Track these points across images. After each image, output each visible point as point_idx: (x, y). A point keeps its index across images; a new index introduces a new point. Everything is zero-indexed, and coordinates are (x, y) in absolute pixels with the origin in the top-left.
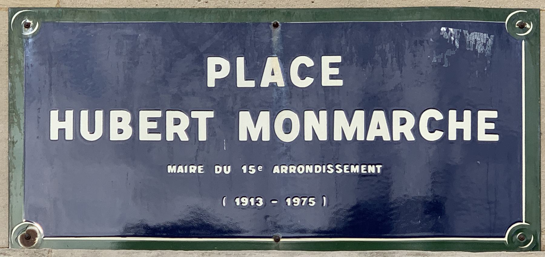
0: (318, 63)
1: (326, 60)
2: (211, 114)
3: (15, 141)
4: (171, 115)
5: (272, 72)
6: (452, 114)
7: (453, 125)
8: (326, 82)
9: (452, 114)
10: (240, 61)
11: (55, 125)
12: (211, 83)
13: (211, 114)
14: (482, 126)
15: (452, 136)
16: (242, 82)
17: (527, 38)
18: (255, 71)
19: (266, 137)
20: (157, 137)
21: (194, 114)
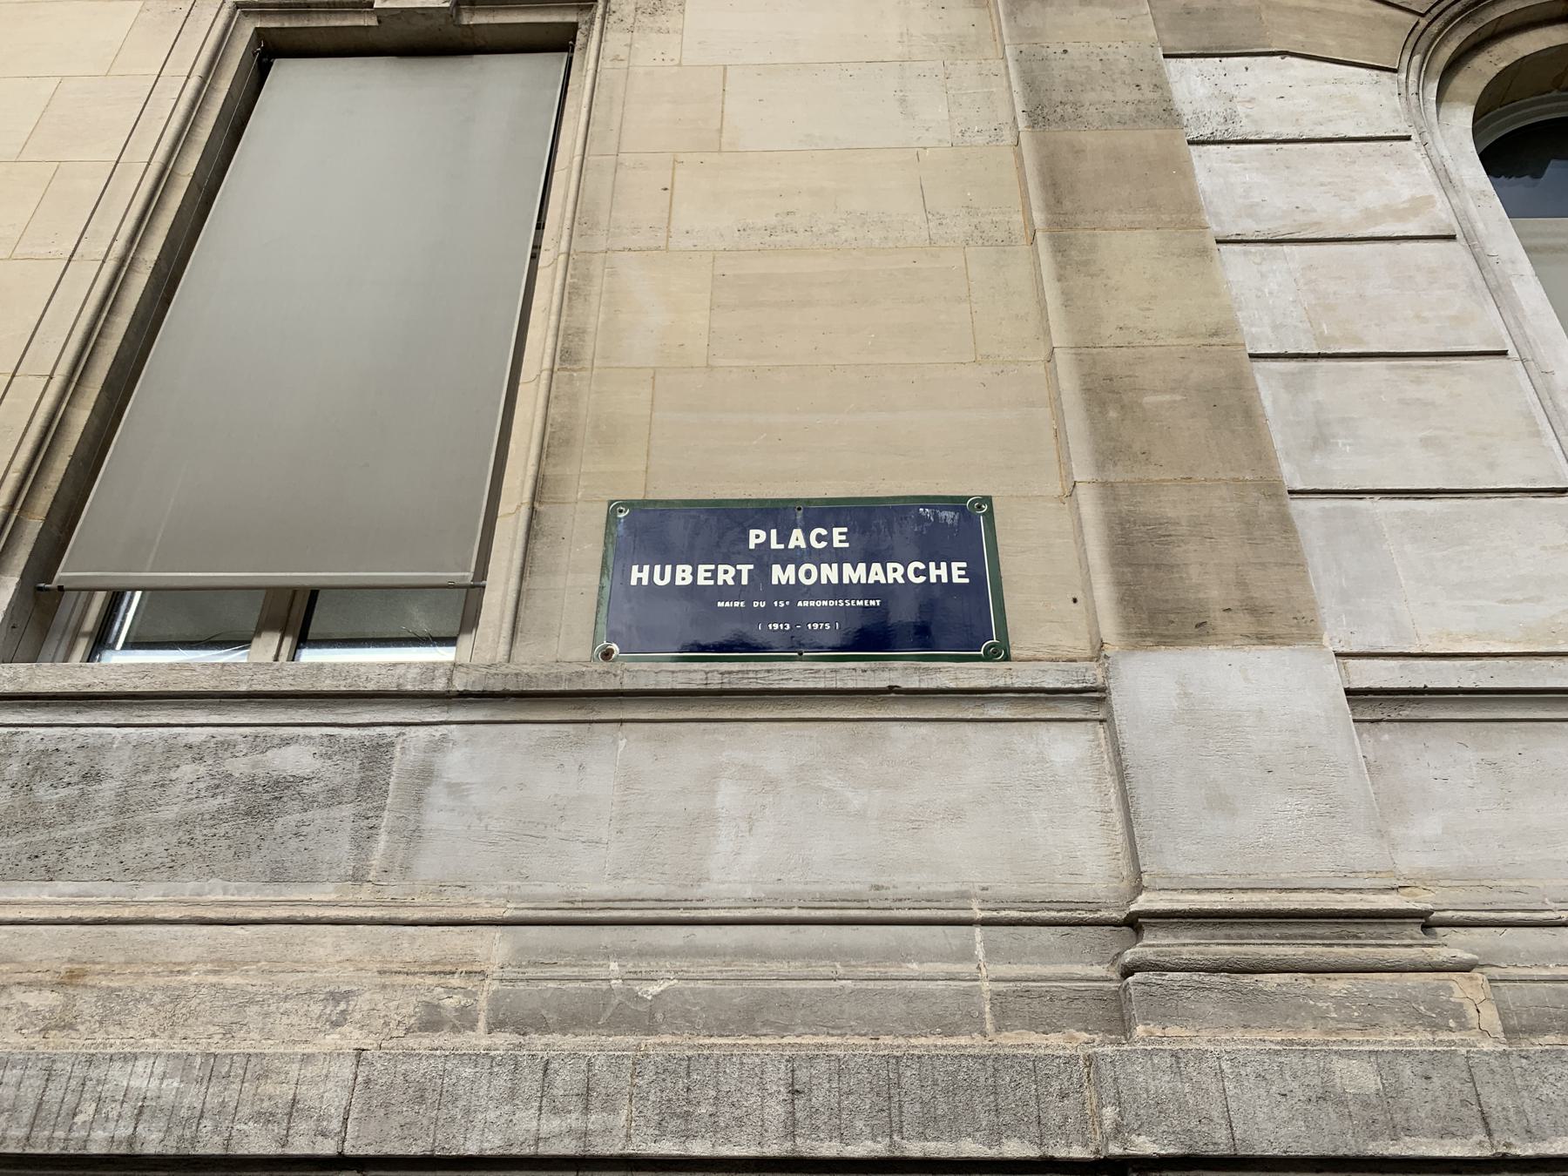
0: (831, 533)
1: (836, 531)
4: (721, 568)
5: (797, 539)
7: (933, 573)
12: (752, 546)
14: (955, 573)
18: (784, 538)
19: (792, 582)
20: (711, 582)
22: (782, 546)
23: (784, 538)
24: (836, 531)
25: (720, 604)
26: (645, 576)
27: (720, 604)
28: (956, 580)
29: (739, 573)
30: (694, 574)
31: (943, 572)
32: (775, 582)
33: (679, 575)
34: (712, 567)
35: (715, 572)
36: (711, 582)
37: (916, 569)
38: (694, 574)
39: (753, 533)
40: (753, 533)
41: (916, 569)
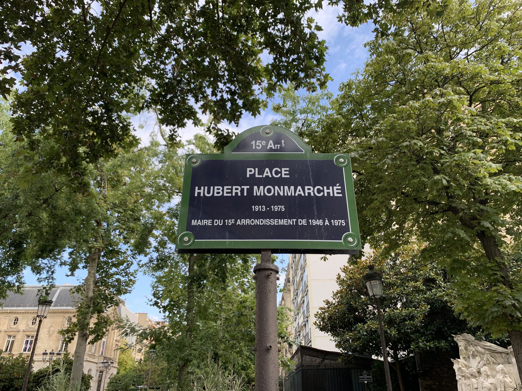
0: (281, 170)
1: (283, 169)
2: (248, 187)
3: (53, 197)
4: (234, 187)
5: (267, 172)
6: (325, 187)
7: (326, 191)
8: (283, 176)
9: (325, 187)
10: (257, 169)
11: (197, 191)
12: (248, 176)
13: (248, 187)
14: (335, 191)
15: (234, 194)
16: (257, 176)
17: (345, 167)
18: (261, 172)
19: (262, 194)
20: (230, 195)
21: (242, 187)
22: (242, 187)
23: (261, 172)
24: (283, 169)
25: (374, 357)
26: (202, 191)
27: (374, 357)
28: (336, 195)
29: (242, 190)
30: (143, 54)
31: (331, 191)
32: (255, 194)
33: (216, 191)
34: (230, 187)
35: (232, 189)
36: (230, 195)
37: (318, 189)
38: (143, 54)
39: (248, 169)
40: (248, 169)
41: (318, 189)
